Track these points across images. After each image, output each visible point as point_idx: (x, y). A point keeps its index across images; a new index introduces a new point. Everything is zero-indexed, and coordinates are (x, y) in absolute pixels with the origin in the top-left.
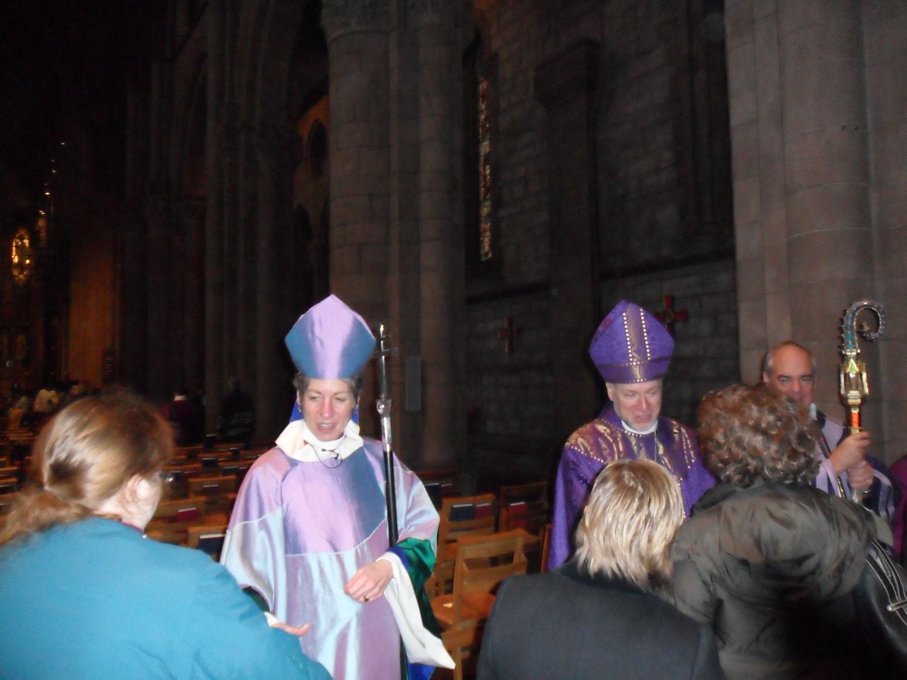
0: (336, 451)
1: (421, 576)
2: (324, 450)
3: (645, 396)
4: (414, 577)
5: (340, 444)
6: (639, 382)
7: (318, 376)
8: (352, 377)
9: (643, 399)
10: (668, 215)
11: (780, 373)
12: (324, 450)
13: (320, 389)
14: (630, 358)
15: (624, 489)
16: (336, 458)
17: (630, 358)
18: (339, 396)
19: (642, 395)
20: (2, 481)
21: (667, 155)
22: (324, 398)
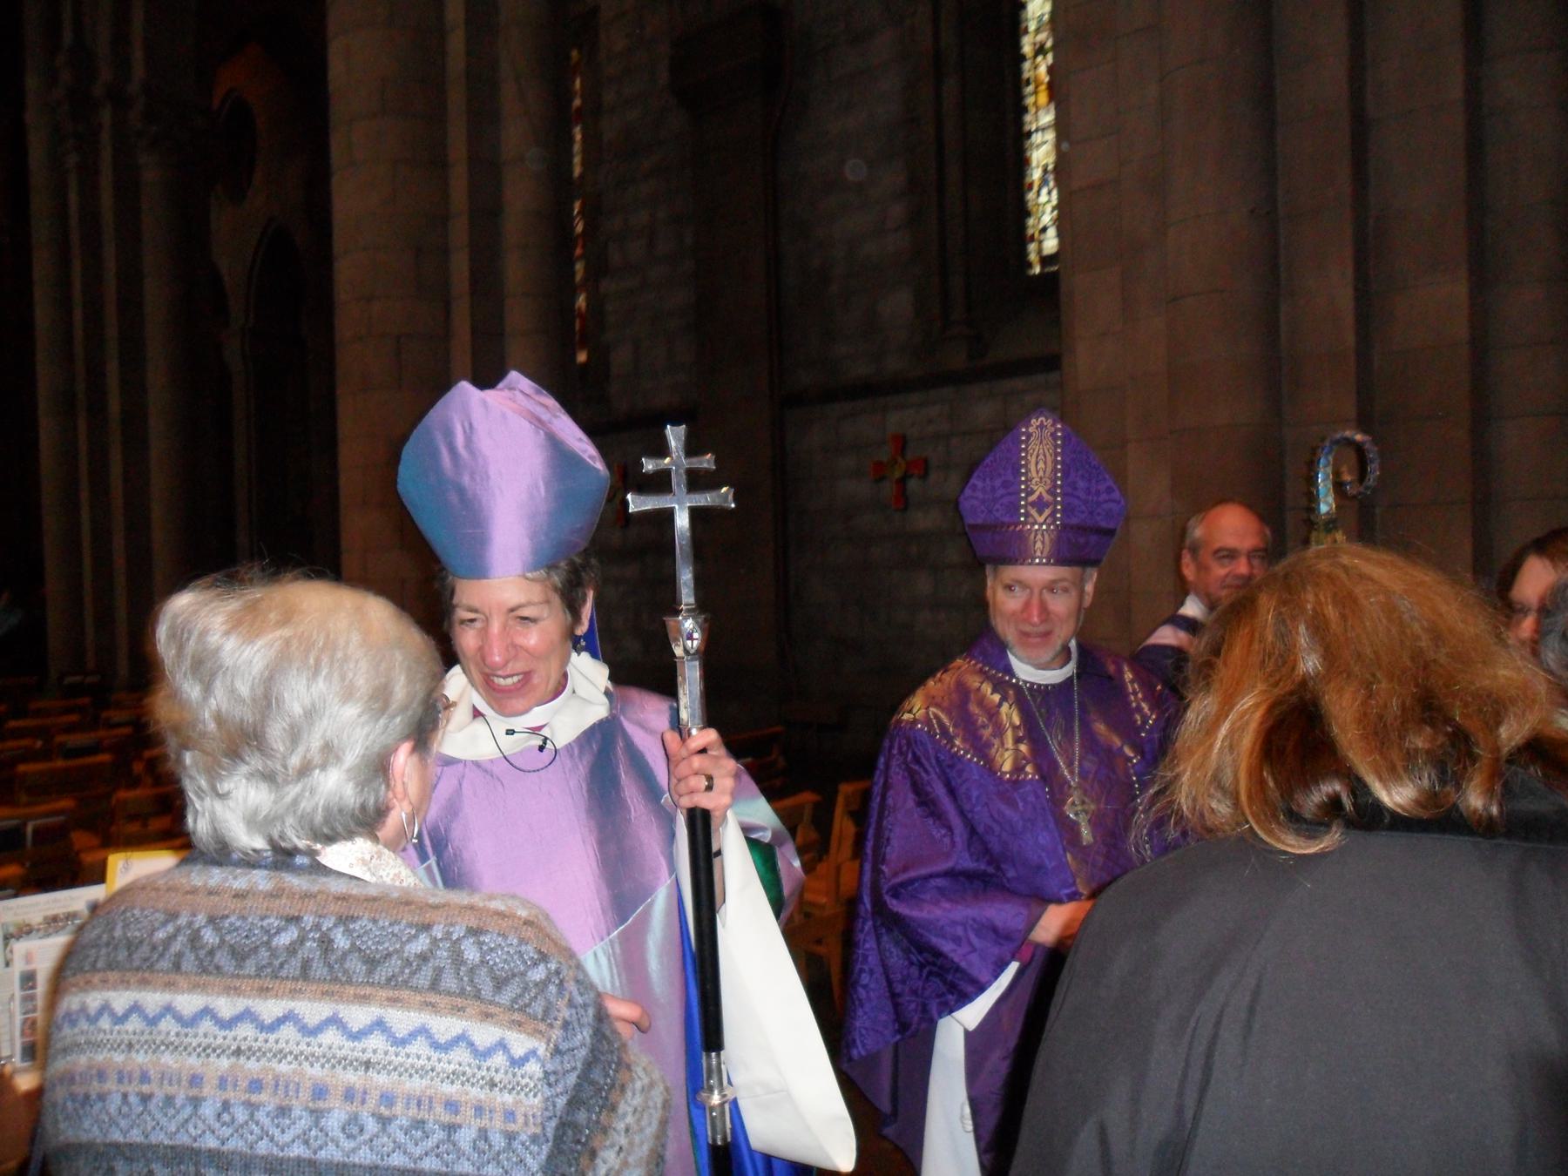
0: (544, 732)
1: (581, 977)
2: (510, 732)
3: (1041, 593)
4: (992, 1120)
5: (556, 712)
6: (1038, 564)
7: (479, 571)
8: (551, 567)
9: (1035, 601)
10: (898, 305)
11: (1217, 545)
12: (510, 732)
13: (476, 603)
14: (1022, 515)
15: (215, 771)
16: (541, 748)
17: (1022, 515)
18: (526, 612)
19: (1036, 591)
20: (455, 10)
21: (897, 211)
22: (487, 620)
